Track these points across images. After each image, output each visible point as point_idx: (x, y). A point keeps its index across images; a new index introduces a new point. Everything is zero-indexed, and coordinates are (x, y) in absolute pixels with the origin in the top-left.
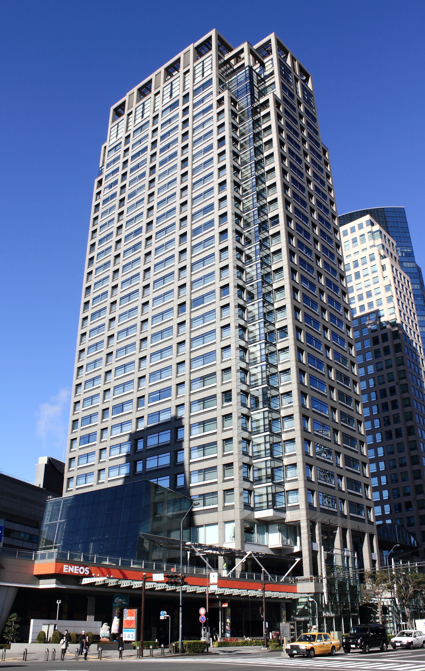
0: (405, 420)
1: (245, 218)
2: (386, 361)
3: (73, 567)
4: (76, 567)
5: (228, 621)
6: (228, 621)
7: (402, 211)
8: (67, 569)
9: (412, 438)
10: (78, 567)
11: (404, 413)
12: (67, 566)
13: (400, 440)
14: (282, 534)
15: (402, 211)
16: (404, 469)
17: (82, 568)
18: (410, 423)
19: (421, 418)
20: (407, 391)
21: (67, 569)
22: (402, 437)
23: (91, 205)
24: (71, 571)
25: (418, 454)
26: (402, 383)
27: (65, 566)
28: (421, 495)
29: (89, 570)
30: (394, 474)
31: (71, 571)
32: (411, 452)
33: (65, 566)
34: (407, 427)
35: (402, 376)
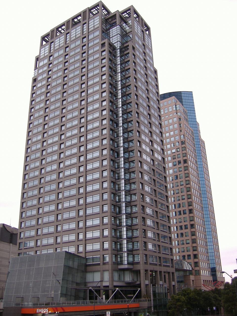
0: (192, 243)
1: (113, 53)
2: (181, 189)
3: (41, 309)
4: (42, 309)
5: (114, 25)
6: (114, 25)
7: (190, 93)
8: (38, 311)
9: (191, 215)
10: (43, 309)
11: (190, 217)
12: (38, 309)
13: (185, 216)
14: (134, 273)
15: (190, 93)
16: (183, 201)
17: (45, 309)
18: (190, 208)
19: (192, 170)
20: (187, 170)
21: (38, 311)
22: (186, 214)
23: (17, 242)
24: (40, 312)
25: (194, 223)
26: (187, 187)
27: (37, 309)
28: (193, 229)
29: (48, 310)
30: (183, 248)
31: (40, 312)
32: (188, 200)
33: (37, 309)
34: (190, 224)
35: (188, 183)
